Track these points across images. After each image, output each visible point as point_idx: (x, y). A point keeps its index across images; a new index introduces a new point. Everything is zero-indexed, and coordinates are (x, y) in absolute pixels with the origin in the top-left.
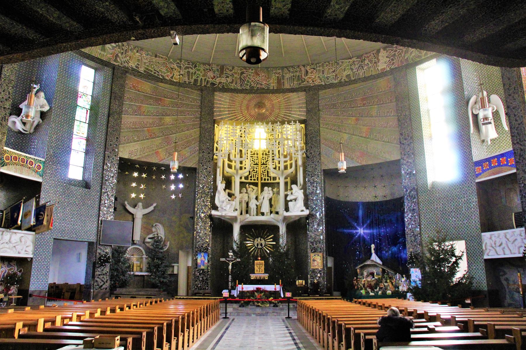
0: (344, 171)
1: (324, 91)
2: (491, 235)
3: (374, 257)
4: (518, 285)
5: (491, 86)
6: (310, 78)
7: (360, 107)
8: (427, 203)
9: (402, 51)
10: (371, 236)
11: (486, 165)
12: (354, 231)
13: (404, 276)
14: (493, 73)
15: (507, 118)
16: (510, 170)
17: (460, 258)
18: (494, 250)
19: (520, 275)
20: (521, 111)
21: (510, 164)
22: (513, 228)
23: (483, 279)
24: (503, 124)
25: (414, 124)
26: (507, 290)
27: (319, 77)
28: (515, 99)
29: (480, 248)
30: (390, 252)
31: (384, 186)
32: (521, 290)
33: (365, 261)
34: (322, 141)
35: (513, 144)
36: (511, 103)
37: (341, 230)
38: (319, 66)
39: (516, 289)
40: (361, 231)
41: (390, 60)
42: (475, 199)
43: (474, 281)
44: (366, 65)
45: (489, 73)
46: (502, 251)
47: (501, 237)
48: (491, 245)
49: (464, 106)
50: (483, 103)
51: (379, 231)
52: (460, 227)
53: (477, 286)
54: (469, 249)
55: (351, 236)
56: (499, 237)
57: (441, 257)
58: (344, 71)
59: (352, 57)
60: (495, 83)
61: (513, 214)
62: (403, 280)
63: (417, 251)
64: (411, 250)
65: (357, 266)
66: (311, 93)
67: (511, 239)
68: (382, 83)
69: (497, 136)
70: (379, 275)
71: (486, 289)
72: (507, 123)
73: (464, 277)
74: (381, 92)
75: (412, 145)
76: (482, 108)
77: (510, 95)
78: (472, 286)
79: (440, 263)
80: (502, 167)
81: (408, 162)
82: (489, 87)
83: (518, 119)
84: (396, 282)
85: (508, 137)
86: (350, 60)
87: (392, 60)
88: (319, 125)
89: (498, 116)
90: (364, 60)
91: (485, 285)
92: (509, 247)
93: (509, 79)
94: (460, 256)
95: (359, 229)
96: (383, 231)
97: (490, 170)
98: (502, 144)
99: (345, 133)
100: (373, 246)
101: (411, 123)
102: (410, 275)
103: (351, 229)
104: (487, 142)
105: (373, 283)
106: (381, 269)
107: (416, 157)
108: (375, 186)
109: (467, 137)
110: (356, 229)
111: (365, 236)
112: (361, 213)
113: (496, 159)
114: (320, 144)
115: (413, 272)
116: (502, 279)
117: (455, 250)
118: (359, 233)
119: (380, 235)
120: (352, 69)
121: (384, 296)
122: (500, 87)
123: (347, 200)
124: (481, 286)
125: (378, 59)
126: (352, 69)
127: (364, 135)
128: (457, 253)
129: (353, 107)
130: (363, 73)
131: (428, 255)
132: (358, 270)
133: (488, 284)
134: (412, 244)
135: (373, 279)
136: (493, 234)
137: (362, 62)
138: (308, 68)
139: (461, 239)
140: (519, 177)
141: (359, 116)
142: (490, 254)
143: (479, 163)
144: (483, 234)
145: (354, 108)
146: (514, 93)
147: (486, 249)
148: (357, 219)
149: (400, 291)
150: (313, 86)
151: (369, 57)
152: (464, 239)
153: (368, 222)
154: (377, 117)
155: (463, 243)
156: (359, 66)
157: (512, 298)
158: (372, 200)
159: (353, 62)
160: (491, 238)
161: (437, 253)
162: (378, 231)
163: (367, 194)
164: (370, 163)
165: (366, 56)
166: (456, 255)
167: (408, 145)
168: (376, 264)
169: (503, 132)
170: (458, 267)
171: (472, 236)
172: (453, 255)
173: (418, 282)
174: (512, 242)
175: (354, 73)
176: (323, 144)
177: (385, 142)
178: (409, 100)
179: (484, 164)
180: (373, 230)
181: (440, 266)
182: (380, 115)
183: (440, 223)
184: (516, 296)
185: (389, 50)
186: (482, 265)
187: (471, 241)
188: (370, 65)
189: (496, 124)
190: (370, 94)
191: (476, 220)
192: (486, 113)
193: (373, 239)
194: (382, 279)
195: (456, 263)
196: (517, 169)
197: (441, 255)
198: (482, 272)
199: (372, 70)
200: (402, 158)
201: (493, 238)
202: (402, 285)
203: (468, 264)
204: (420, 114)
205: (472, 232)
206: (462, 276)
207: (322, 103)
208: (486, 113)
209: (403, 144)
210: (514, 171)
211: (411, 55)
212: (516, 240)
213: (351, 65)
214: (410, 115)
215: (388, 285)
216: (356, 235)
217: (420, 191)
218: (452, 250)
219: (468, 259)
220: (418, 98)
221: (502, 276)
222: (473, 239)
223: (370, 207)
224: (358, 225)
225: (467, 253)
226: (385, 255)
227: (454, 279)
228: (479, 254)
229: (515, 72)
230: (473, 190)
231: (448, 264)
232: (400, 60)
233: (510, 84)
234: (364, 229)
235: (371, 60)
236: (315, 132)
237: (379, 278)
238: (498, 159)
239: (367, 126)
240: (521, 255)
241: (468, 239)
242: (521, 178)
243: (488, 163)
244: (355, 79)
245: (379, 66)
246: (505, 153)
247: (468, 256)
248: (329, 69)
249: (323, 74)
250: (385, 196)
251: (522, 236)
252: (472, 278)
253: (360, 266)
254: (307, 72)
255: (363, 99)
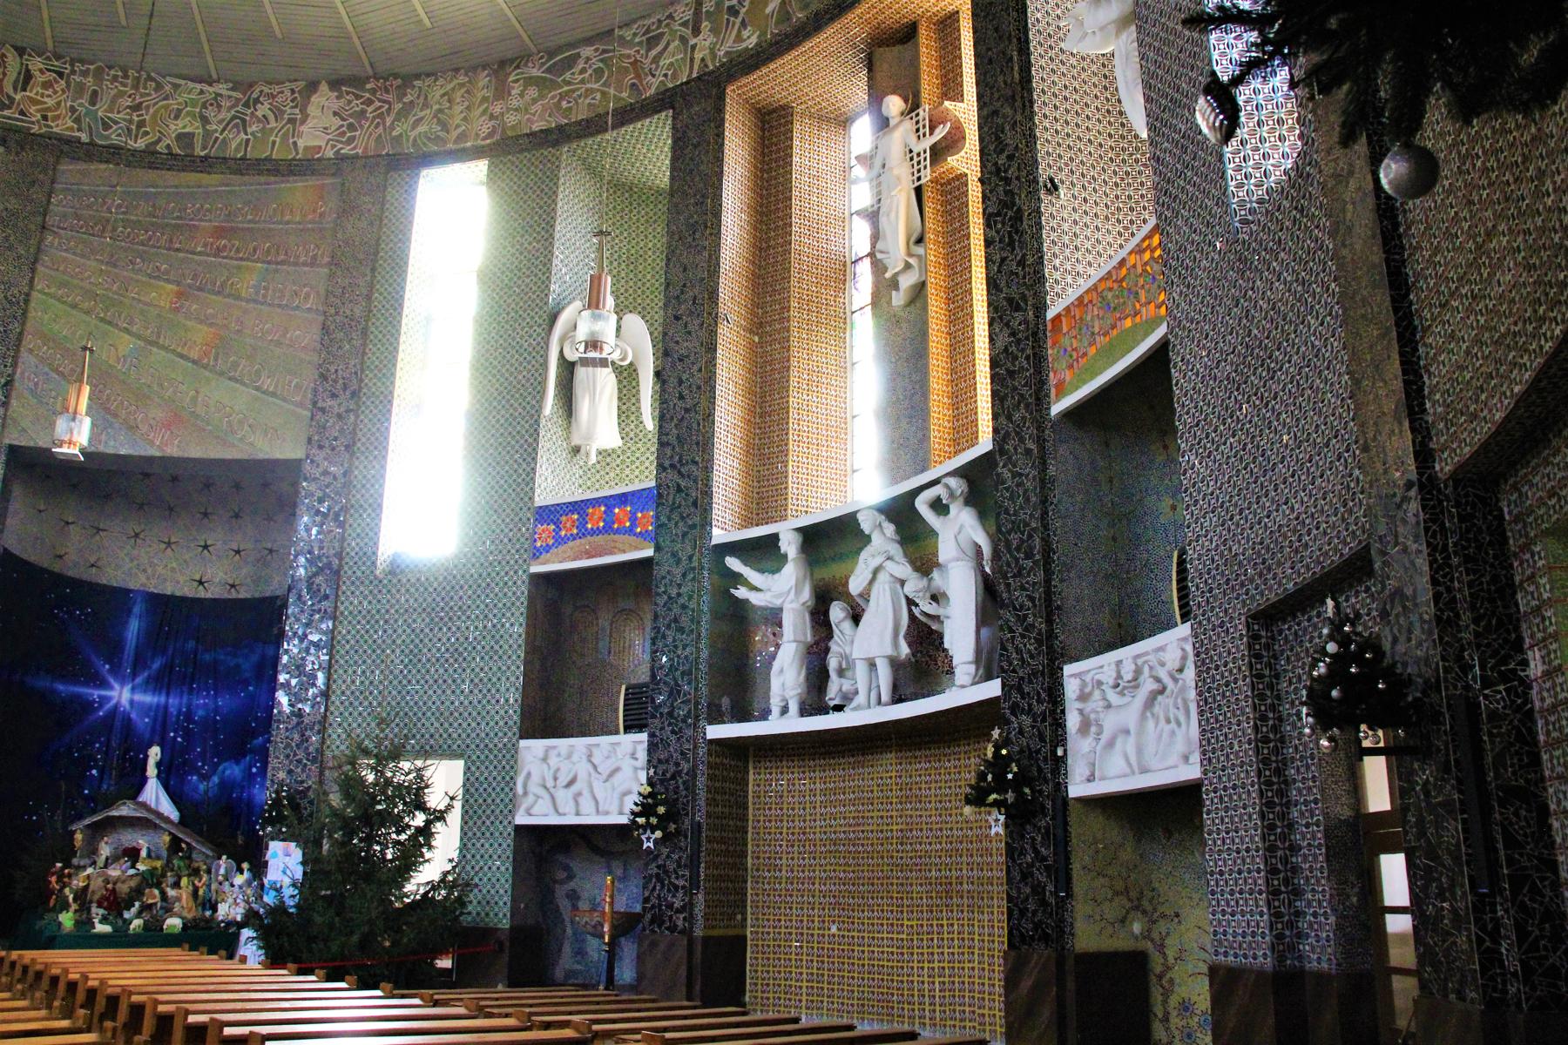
0: (76, 451)
1: (81, 166)
2: (548, 750)
3: (154, 794)
4: (603, 913)
5: (631, 291)
6: (34, 102)
7: (200, 253)
8: (364, 622)
9: (390, 109)
10: (155, 720)
11: (568, 525)
12: (96, 694)
13: (245, 866)
14: (645, 252)
15: (657, 388)
16: (637, 548)
17: (440, 816)
18: (547, 797)
19: (613, 882)
20: (700, 370)
21: (639, 530)
22: (617, 733)
23: (502, 892)
24: (643, 410)
25: (374, 354)
26: (569, 931)
27: (73, 110)
28: (689, 333)
29: (507, 789)
30: (216, 779)
31: (238, 552)
32: (606, 929)
33: (110, 805)
34: (29, 341)
35: (661, 467)
36: (677, 342)
37: (43, 683)
38: (85, 73)
39: (594, 927)
40: (122, 695)
41: (342, 126)
42: (516, 627)
43: (473, 896)
44: (259, 121)
45: (633, 251)
46: (572, 803)
47: (575, 758)
48: (544, 779)
49: (540, 325)
50: (595, 294)
51: (189, 706)
52: (456, 714)
53: (478, 914)
54: (472, 790)
55: (87, 706)
56: (569, 756)
57: (379, 807)
58: (176, 117)
59: (215, 76)
60: (644, 284)
61: (624, 687)
62: (239, 880)
63: (302, 782)
64: (282, 775)
65: (80, 817)
66: (28, 156)
67: (605, 768)
68: (297, 192)
69: (620, 443)
70: (158, 858)
71: (505, 924)
72: (654, 409)
73: (443, 880)
74: (288, 223)
75: (352, 418)
76: (589, 307)
77: (677, 318)
78: (462, 914)
79: (372, 830)
80: (616, 537)
81: (326, 473)
82: (626, 291)
83: (686, 392)
84: (209, 886)
85: (648, 455)
86: (206, 87)
87: (351, 127)
88: (32, 280)
89: (634, 384)
90: (257, 101)
91: (507, 910)
92: (595, 791)
93: (685, 270)
94: (440, 811)
95: (117, 686)
96: (205, 704)
97: (578, 541)
98: (627, 471)
99: (127, 331)
100: (155, 753)
101: (364, 345)
102: (267, 862)
103: (86, 684)
104: (587, 454)
105: (124, 889)
106: (167, 838)
107: (357, 463)
108: (206, 547)
109: (531, 426)
110: (104, 684)
111: (133, 716)
112: (133, 628)
113: (603, 509)
114: (17, 351)
115: (275, 855)
116: (560, 892)
117: (427, 786)
118: (114, 702)
119: (189, 716)
120: (205, 120)
121: (154, 937)
122: (656, 300)
123: (91, 575)
124: (492, 914)
125: (303, 111)
126: (205, 120)
127: (194, 354)
128: (435, 800)
129: (178, 250)
130: (240, 144)
131: (335, 799)
132: (79, 836)
133: (514, 911)
134: (288, 756)
135: (132, 872)
136: (555, 747)
137: (246, 105)
138: (36, 64)
139: (453, 755)
140: (659, 571)
141: (190, 286)
142: (537, 812)
143: (549, 514)
144: (523, 743)
145: (181, 255)
146: (691, 313)
147: (526, 793)
148: (114, 653)
149: (220, 918)
150: (41, 135)
151: (274, 97)
152: (460, 756)
153: (156, 665)
154: (255, 301)
155: (458, 765)
156: (234, 118)
157: (580, 953)
158: (187, 590)
159: (215, 99)
160: (545, 759)
161: (368, 794)
162: (185, 700)
163: (173, 570)
164: (195, 452)
165: (266, 90)
166: (428, 805)
167: (339, 416)
168: (151, 817)
169: (636, 435)
170: (430, 847)
171: (491, 746)
172: (421, 806)
173: (288, 892)
174: (605, 776)
175: (207, 134)
176: (31, 351)
177: (264, 393)
178: (373, 270)
179: (564, 519)
180: (168, 695)
181: (370, 839)
182: (264, 296)
183: (394, 693)
184: (593, 943)
185: (348, 93)
186: (504, 845)
187: (483, 763)
188: (273, 124)
189: (624, 407)
190: (250, 222)
191: (510, 694)
192: (599, 326)
193: (161, 727)
194: (164, 875)
195: (426, 832)
196: (658, 549)
197: (379, 803)
198: (503, 869)
199: (274, 143)
200: (307, 457)
201: (553, 761)
202: (230, 900)
203: (461, 839)
204: (400, 322)
205: (492, 735)
206: (437, 877)
207: (60, 204)
208: (599, 326)
209: (323, 410)
210: (649, 552)
211: (413, 129)
212: (617, 770)
213: (204, 106)
214: (366, 321)
215: (179, 899)
216: (101, 706)
217: (349, 578)
218: (420, 789)
219: (465, 822)
220: (405, 272)
221: (562, 882)
222: (492, 757)
223: (164, 607)
224: (116, 671)
225: (466, 802)
226: (197, 788)
227: (409, 888)
228: (502, 806)
229: (706, 254)
230: (518, 598)
231: (398, 833)
232: (374, 136)
233: (684, 285)
234: (133, 689)
235: (279, 109)
236: (10, 302)
237: (155, 868)
238: (609, 508)
239: (211, 325)
240: (624, 820)
241: (474, 757)
242: (664, 578)
243: (576, 517)
244: (206, 157)
245: (300, 135)
246: (633, 493)
247: (465, 813)
248: (121, 94)
249: (93, 104)
250: (233, 586)
251: (636, 759)
252: (468, 885)
253: (87, 822)
254: (28, 76)
255: (220, 232)
